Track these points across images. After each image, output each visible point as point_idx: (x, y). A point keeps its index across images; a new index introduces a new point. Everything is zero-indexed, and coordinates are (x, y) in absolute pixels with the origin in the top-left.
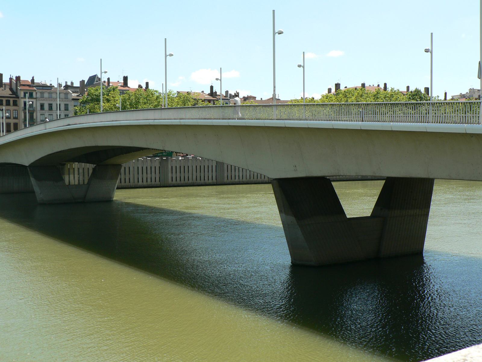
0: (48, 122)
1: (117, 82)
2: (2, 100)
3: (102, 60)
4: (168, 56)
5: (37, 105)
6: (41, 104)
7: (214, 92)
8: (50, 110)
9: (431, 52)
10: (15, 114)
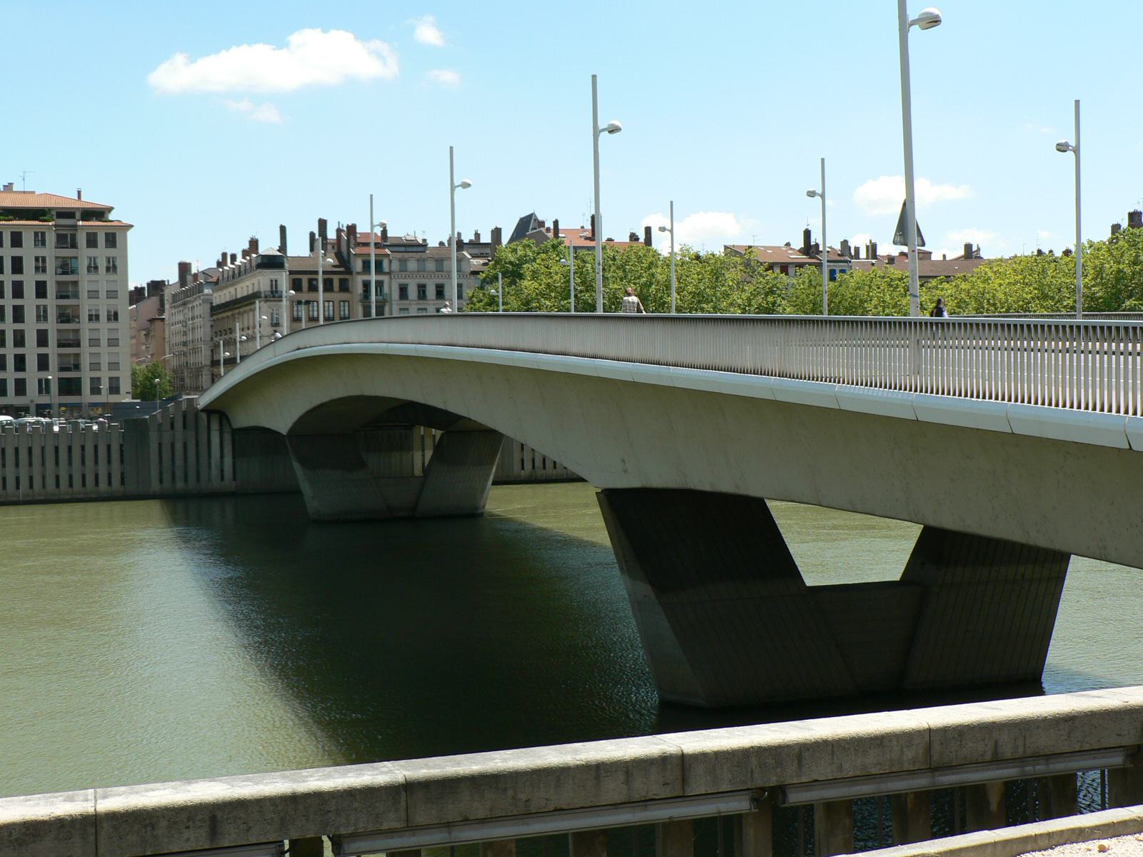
0: (281, 338)
3: (374, 197)
4: (458, 188)
5: (393, 288)
7: (812, 243)
8: (422, 299)
9: (1074, 152)
10: (344, 311)
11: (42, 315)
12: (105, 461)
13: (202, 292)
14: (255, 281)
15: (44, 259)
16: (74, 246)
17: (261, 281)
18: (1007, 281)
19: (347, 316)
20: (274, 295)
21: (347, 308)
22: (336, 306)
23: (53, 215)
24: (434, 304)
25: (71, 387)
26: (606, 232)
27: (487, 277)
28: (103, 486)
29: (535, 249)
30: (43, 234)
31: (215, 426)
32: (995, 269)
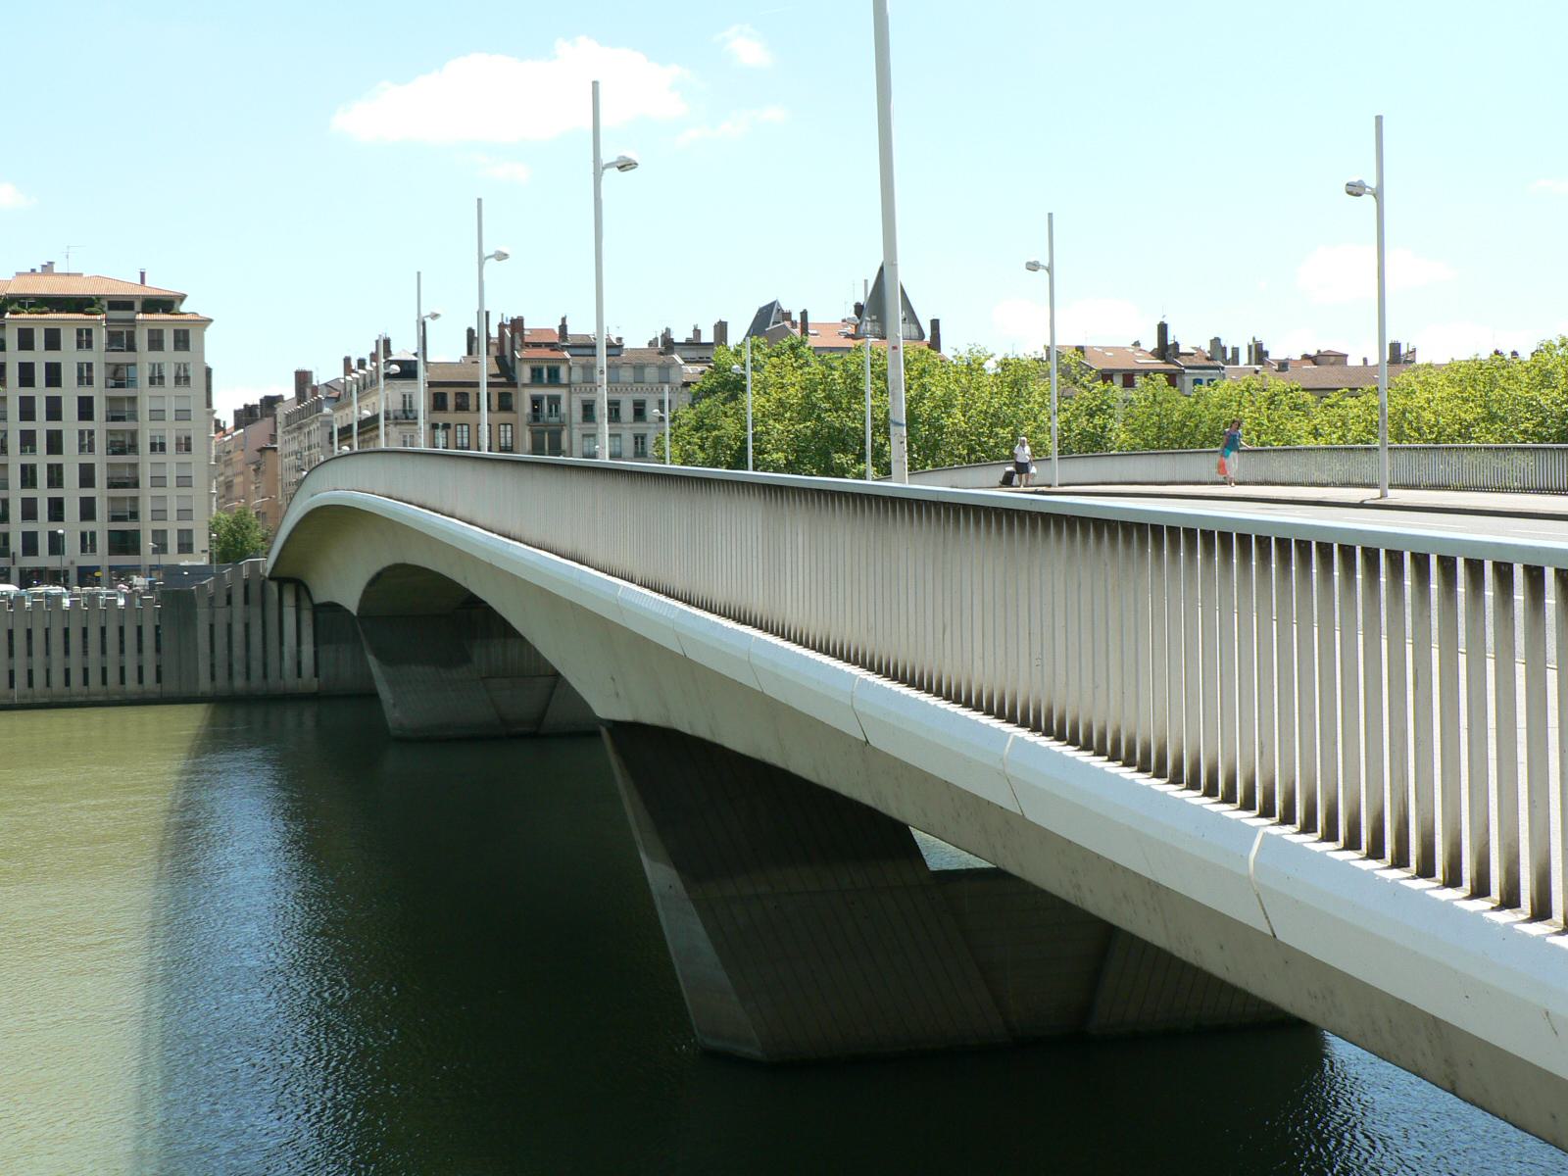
1: (840, 322)
2: (467, 394)
3: (422, 275)
6: (583, 401)
7: (1169, 343)
10: (462, 438)
11: (86, 444)
12: (80, 650)
13: (321, 411)
15: (90, 366)
16: (132, 348)
17: (384, 399)
18: (1438, 395)
19: (466, 445)
20: (405, 416)
21: (465, 434)
23: (103, 306)
24: (631, 428)
25: (123, 543)
27: (700, 389)
28: (131, 684)
29: (767, 351)
30: (89, 332)
31: (289, 600)
32: (1422, 379)
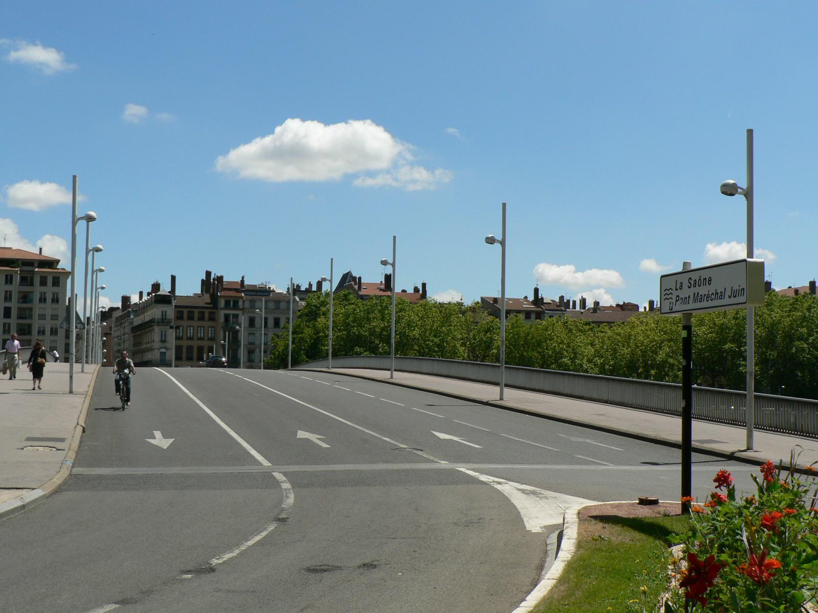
3: (397, 239)
7: (539, 297)
13: (130, 317)
14: (152, 311)
15: (11, 292)
16: (32, 284)
17: (155, 312)
21: (202, 332)
22: (185, 328)
23: (19, 264)
24: (273, 331)
26: (398, 287)
30: (11, 276)
